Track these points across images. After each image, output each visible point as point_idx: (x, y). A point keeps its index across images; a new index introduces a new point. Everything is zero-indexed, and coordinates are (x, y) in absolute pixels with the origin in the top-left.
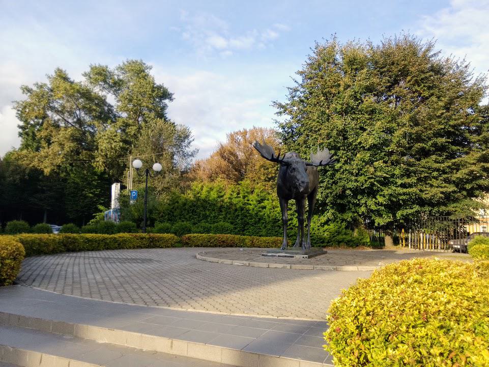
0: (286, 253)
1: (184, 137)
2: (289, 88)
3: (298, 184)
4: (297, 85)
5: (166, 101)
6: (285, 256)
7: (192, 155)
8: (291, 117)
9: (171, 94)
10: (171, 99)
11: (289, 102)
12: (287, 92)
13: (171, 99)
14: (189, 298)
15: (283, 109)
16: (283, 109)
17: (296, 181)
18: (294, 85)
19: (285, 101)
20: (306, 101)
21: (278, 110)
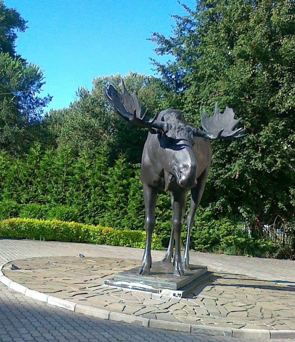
0: (146, 283)
1: (34, 79)
2: (177, 17)
3: (176, 168)
4: (188, 14)
5: (16, 30)
6: (144, 290)
7: (43, 104)
8: (79, 101)
9: (24, 22)
10: (23, 29)
11: (175, 37)
12: (174, 22)
13: (23, 29)
14: (9, 307)
15: (167, 45)
16: (167, 45)
17: (173, 161)
18: (185, 14)
19: (170, 34)
20: (236, 4)
21: (159, 46)
